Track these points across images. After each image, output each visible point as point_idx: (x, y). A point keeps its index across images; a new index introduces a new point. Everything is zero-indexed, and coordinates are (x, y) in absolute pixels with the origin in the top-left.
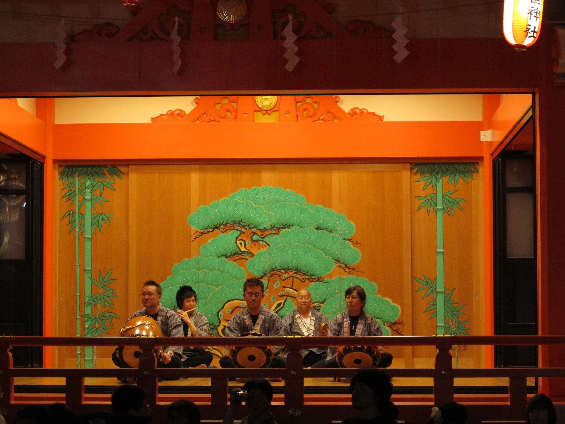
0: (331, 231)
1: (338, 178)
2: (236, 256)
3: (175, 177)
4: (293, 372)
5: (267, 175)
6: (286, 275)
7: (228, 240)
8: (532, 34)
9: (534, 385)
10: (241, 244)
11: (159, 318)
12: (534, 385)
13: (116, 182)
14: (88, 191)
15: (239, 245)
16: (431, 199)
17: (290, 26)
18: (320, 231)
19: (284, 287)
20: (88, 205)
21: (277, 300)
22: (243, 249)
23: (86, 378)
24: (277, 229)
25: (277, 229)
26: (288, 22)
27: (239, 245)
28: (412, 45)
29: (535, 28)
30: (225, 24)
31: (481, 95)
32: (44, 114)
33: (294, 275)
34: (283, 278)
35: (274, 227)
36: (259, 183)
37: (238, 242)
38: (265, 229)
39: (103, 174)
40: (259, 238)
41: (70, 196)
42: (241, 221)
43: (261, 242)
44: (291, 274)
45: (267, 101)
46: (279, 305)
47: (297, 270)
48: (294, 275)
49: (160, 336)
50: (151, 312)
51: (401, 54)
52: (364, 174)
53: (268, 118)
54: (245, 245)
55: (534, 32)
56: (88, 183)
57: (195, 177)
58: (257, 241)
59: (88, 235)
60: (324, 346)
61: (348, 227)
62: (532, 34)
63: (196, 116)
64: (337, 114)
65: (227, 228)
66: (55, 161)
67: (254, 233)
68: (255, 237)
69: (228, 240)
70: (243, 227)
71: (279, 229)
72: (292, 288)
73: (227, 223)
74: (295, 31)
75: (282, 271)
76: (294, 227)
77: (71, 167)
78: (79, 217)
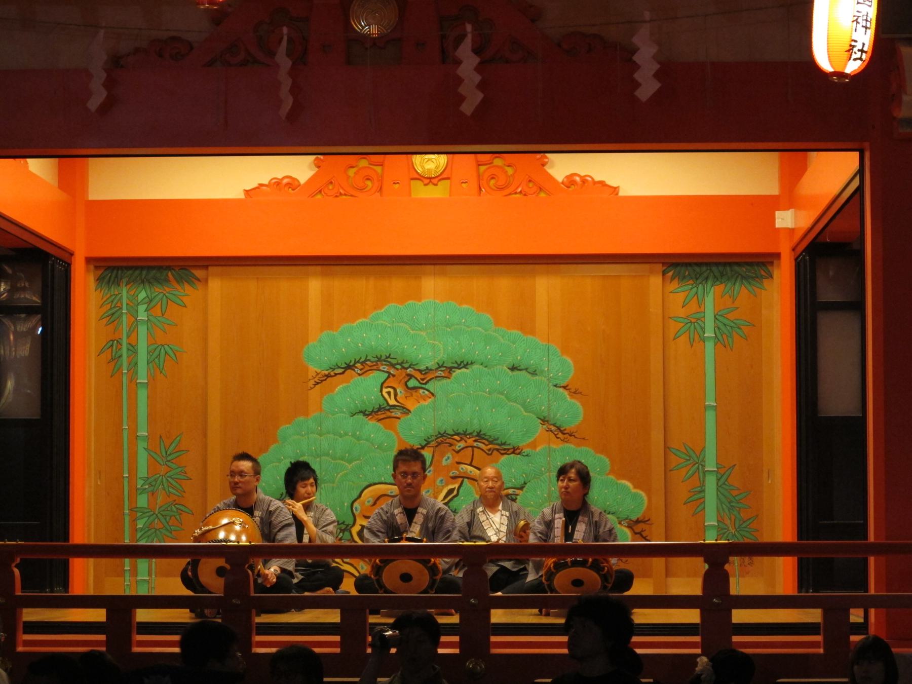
0: (534, 373)
1: (546, 287)
2: (381, 413)
3: (283, 285)
4: (472, 601)
5: (431, 283)
6: (462, 444)
7: (367, 388)
8: (858, 55)
9: (862, 620)
10: (389, 393)
11: (257, 513)
12: (862, 620)
13: (188, 293)
14: (142, 308)
15: (386, 396)
16: (696, 321)
17: (468, 42)
18: (516, 373)
19: (459, 463)
20: (142, 331)
21: (447, 484)
22: (392, 402)
23: (138, 610)
24: (447, 370)
25: (447, 370)
26: (464, 36)
27: (386, 396)
28: (665, 72)
29: (864, 44)
30: (362, 39)
31: (777, 153)
32: (71, 184)
33: (475, 444)
34: (457, 448)
35: (442, 366)
36: (418, 296)
37: (385, 390)
38: (428, 370)
39: (167, 280)
40: (417, 384)
41: (112, 316)
42: (389, 357)
43: (421, 391)
44: (470, 441)
45: (431, 163)
46: (450, 492)
47: (480, 436)
48: (475, 444)
49: (258, 542)
50: (244, 503)
51: (648, 86)
52: (587, 281)
53: (433, 191)
54: (396, 395)
55: (862, 51)
56: (142, 295)
57: (315, 286)
58: (415, 388)
59: (142, 378)
60: (524, 557)
61: (562, 367)
62: (858, 55)
63: (316, 187)
64: (545, 184)
65: (367, 368)
66: (89, 260)
67: (410, 376)
68: (412, 383)
69: (367, 388)
70: (393, 366)
71: (450, 370)
72: (471, 465)
73: (366, 360)
74: (477, 51)
75: (455, 437)
76: (475, 367)
77: (114, 270)
78: (128, 349)
